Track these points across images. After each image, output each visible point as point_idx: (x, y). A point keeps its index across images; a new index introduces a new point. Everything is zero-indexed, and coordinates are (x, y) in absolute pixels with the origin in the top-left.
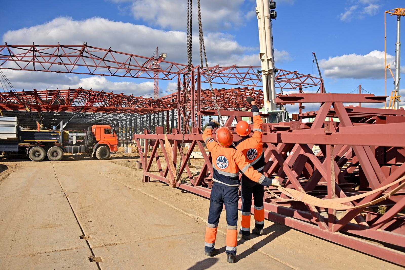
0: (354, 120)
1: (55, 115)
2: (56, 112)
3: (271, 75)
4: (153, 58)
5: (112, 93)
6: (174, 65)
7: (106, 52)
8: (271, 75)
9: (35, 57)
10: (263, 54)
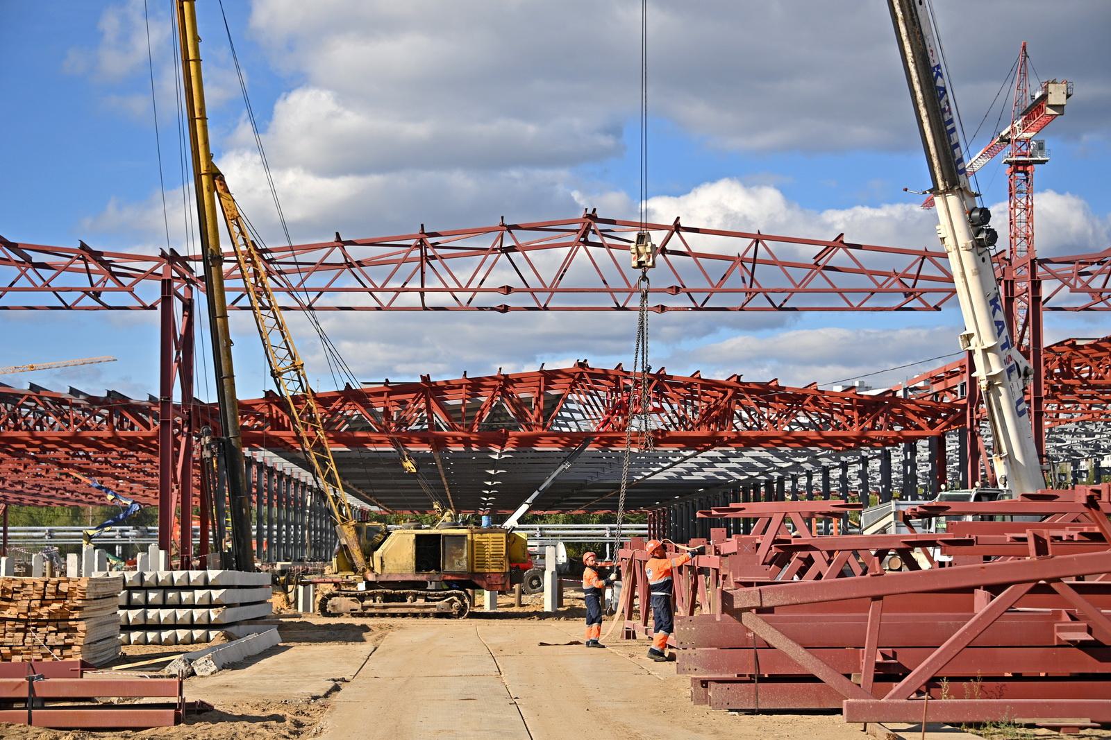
0: (764, 532)
1: (496, 457)
2: (498, 451)
3: (1000, 388)
4: (842, 242)
5: (697, 376)
6: (926, 260)
7: (666, 233)
8: (1000, 388)
9: (424, 261)
10: (972, 335)
